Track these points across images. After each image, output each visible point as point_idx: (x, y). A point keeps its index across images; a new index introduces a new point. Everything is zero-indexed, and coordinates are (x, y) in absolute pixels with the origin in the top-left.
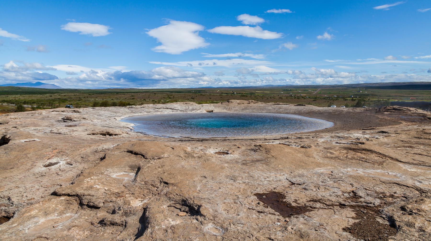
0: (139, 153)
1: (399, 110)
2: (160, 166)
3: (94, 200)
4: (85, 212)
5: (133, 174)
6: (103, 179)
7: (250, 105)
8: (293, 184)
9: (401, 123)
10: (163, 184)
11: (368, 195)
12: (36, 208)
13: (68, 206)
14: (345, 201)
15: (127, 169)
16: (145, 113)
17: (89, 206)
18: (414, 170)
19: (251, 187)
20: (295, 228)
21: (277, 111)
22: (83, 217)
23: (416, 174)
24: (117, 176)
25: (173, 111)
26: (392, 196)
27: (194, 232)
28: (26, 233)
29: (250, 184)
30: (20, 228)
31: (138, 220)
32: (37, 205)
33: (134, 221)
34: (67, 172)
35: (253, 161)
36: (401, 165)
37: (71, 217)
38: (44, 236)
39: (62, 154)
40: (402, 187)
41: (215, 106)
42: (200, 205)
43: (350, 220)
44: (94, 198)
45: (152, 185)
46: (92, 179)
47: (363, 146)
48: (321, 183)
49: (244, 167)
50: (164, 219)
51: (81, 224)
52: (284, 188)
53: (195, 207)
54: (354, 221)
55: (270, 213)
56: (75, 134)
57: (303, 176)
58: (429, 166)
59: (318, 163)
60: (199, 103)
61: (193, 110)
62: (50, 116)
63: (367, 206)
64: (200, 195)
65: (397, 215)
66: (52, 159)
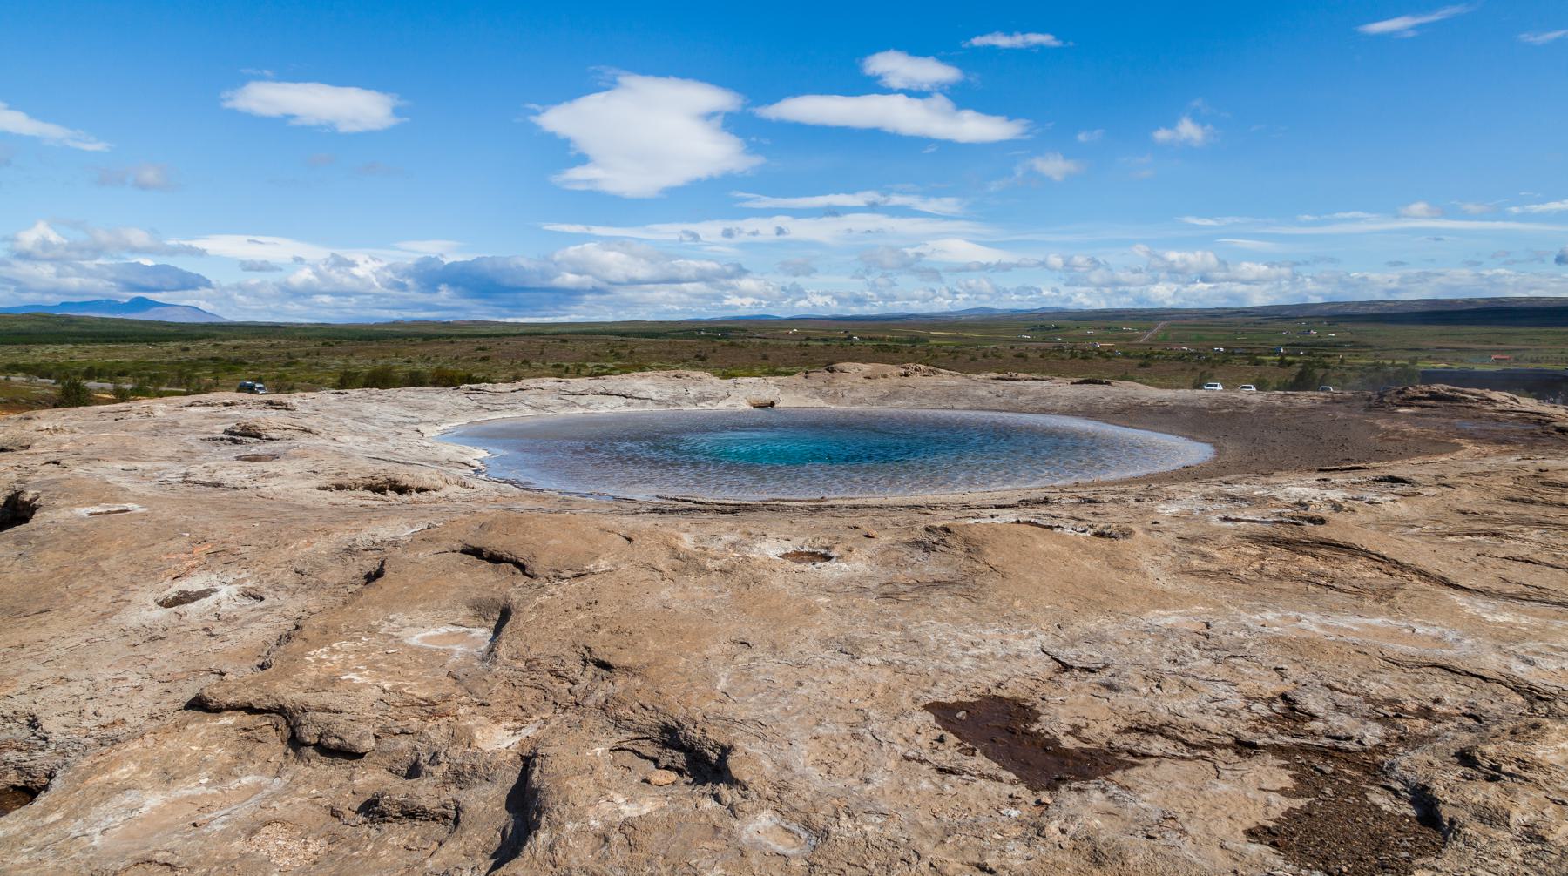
0: (506, 555)
1: (1453, 399)
2: (583, 604)
3: (342, 727)
4: (310, 770)
5: (483, 634)
6: (375, 649)
7: (909, 381)
8: (1066, 668)
9: (1458, 447)
10: (591, 668)
11: (1338, 708)
12: (130, 757)
13: (248, 748)
14: (1256, 730)
15: (462, 613)
16: (529, 412)
17: (324, 750)
18: (1505, 618)
19: (914, 679)
20: (1072, 829)
21: (1007, 402)
22: (302, 790)
23: (1512, 632)
24: (424, 639)
25: (629, 405)
26: (1426, 713)
27: (707, 845)
28: (95, 848)
29: (910, 669)
30: (74, 828)
31: (504, 798)
32: (135, 746)
33: (486, 805)
34: (242, 626)
35: (919, 586)
36: (1459, 599)
37: (259, 788)
38: (158, 856)
39: (224, 558)
40: (1462, 679)
41: (782, 387)
42: (726, 744)
43: (1274, 798)
44: (341, 719)
45: (554, 673)
46: (333, 651)
47: (1321, 532)
48: (1167, 667)
49: (889, 607)
50: (595, 795)
51: (296, 814)
52: (1032, 684)
53: (710, 753)
54: (1287, 803)
55: (982, 776)
56: (272, 487)
57: (1103, 639)
58: (1559, 604)
59: (1156, 592)
60: (725, 376)
61: (702, 399)
62: (182, 423)
63: (1337, 749)
64: (729, 709)
65: (1446, 783)
66: (190, 580)
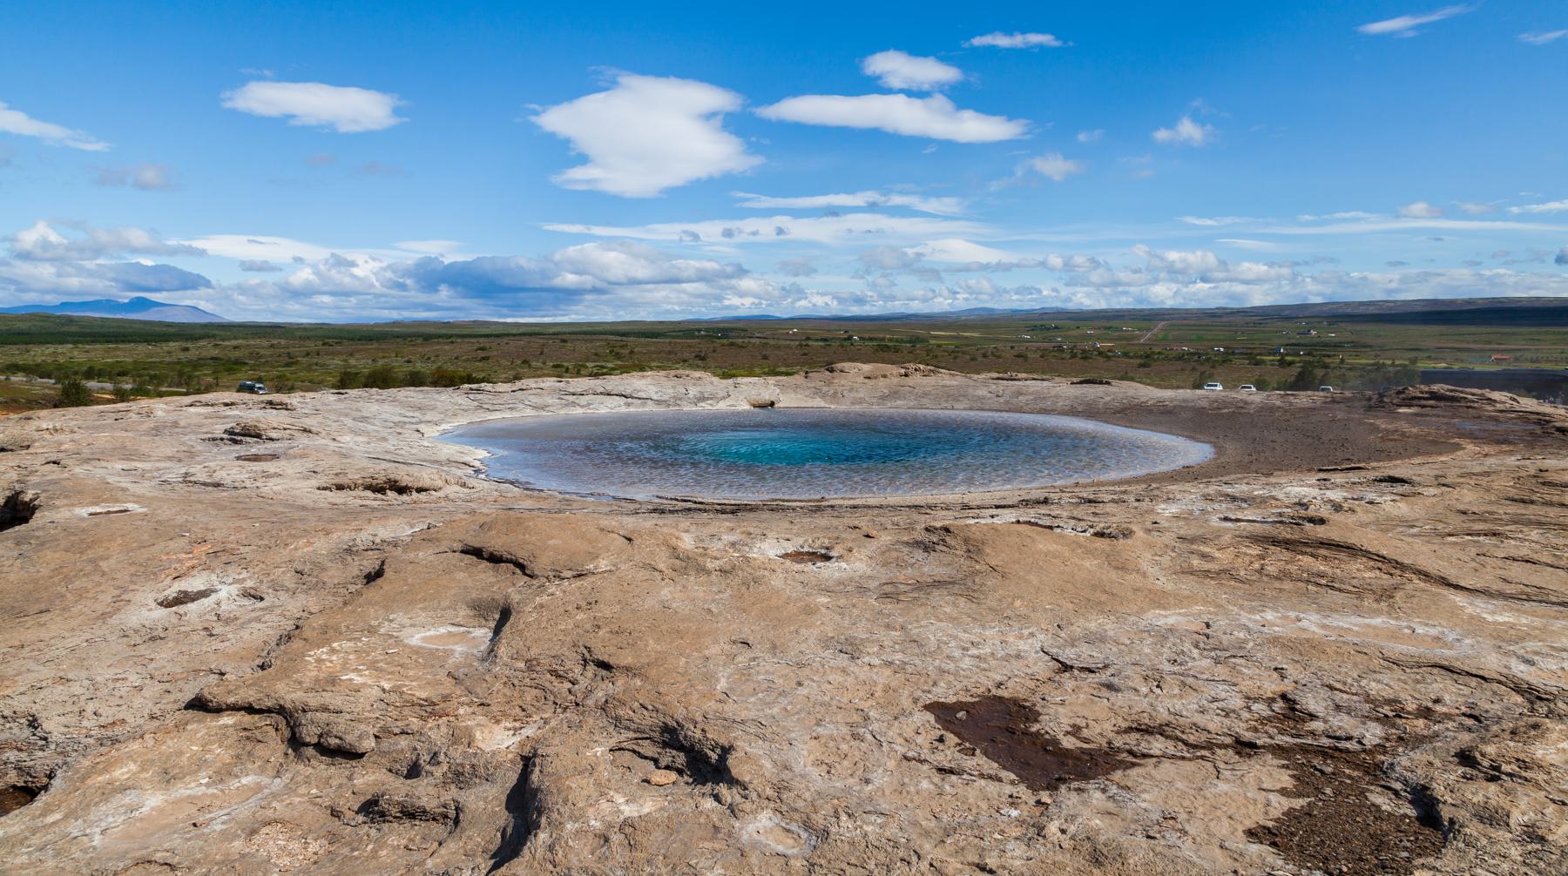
0: (506, 555)
1: (1453, 399)
2: (583, 604)
3: (342, 727)
4: (310, 770)
5: (483, 634)
6: (375, 649)
7: (909, 381)
8: (1066, 668)
9: (1458, 447)
10: (591, 668)
11: (1338, 708)
12: (130, 757)
13: (248, 748)
14: (1256, 730)
15: (462, 613)
16: (529, 412)
17: (324, 750)
18: (1505, 618)
19: (914, 679)
20: (1072, 829)
21: (1007, 402)
22: (302, 790)
23: (1512, 632)
24: (424, 639)
25: (629, 405)
26: (1426, 713)
27: (707, 845)
28: (95, 848)
29: (910, 669)
30: (74, 828)
31: (504, 798)
32: (135, 746)
33: (486, 805)
34: (242, 626)
35: (919, 586)
36: (1459, 599)
37: (259, 788)
38: (158, 856)
39: (224, 558)
40: (1462, 679)
41: (782, 387)
42: (726, 744)
43: (1274, 798)
44: (341, 719)
45: (554, 673)
46: (333, 651)
47: (1321, 532)
48: (1167, 667)
49: (889, 607)
50: (595, 795)
51: (296, 814)
52: (1032, 684)
53: (710, 753)
54: (1287, 803)
55: (982, 776)
56: (272, 487)
57: (1103, 639)
58: (1559, 604)
59: (1156, 592)
60: (725, 376)
61: (702, 399)
62: (182, 423)
63: (1337, 749)
64: (729, 709)
65: (1446, 783)
66: (190, 580)
